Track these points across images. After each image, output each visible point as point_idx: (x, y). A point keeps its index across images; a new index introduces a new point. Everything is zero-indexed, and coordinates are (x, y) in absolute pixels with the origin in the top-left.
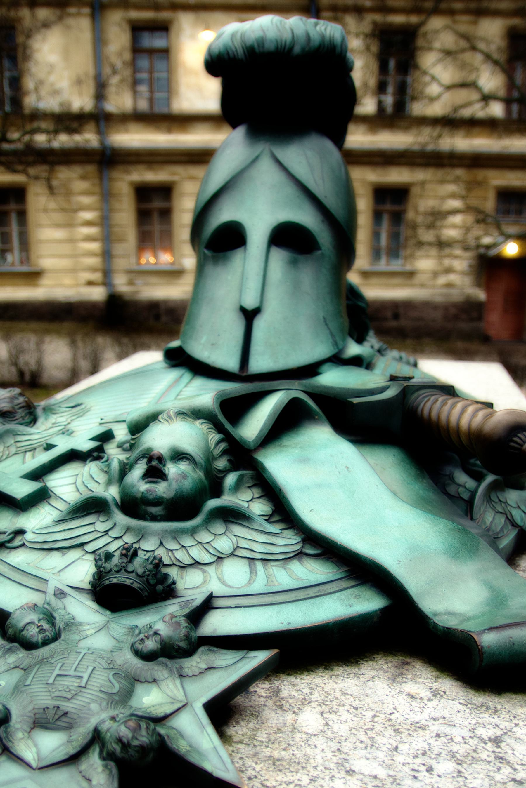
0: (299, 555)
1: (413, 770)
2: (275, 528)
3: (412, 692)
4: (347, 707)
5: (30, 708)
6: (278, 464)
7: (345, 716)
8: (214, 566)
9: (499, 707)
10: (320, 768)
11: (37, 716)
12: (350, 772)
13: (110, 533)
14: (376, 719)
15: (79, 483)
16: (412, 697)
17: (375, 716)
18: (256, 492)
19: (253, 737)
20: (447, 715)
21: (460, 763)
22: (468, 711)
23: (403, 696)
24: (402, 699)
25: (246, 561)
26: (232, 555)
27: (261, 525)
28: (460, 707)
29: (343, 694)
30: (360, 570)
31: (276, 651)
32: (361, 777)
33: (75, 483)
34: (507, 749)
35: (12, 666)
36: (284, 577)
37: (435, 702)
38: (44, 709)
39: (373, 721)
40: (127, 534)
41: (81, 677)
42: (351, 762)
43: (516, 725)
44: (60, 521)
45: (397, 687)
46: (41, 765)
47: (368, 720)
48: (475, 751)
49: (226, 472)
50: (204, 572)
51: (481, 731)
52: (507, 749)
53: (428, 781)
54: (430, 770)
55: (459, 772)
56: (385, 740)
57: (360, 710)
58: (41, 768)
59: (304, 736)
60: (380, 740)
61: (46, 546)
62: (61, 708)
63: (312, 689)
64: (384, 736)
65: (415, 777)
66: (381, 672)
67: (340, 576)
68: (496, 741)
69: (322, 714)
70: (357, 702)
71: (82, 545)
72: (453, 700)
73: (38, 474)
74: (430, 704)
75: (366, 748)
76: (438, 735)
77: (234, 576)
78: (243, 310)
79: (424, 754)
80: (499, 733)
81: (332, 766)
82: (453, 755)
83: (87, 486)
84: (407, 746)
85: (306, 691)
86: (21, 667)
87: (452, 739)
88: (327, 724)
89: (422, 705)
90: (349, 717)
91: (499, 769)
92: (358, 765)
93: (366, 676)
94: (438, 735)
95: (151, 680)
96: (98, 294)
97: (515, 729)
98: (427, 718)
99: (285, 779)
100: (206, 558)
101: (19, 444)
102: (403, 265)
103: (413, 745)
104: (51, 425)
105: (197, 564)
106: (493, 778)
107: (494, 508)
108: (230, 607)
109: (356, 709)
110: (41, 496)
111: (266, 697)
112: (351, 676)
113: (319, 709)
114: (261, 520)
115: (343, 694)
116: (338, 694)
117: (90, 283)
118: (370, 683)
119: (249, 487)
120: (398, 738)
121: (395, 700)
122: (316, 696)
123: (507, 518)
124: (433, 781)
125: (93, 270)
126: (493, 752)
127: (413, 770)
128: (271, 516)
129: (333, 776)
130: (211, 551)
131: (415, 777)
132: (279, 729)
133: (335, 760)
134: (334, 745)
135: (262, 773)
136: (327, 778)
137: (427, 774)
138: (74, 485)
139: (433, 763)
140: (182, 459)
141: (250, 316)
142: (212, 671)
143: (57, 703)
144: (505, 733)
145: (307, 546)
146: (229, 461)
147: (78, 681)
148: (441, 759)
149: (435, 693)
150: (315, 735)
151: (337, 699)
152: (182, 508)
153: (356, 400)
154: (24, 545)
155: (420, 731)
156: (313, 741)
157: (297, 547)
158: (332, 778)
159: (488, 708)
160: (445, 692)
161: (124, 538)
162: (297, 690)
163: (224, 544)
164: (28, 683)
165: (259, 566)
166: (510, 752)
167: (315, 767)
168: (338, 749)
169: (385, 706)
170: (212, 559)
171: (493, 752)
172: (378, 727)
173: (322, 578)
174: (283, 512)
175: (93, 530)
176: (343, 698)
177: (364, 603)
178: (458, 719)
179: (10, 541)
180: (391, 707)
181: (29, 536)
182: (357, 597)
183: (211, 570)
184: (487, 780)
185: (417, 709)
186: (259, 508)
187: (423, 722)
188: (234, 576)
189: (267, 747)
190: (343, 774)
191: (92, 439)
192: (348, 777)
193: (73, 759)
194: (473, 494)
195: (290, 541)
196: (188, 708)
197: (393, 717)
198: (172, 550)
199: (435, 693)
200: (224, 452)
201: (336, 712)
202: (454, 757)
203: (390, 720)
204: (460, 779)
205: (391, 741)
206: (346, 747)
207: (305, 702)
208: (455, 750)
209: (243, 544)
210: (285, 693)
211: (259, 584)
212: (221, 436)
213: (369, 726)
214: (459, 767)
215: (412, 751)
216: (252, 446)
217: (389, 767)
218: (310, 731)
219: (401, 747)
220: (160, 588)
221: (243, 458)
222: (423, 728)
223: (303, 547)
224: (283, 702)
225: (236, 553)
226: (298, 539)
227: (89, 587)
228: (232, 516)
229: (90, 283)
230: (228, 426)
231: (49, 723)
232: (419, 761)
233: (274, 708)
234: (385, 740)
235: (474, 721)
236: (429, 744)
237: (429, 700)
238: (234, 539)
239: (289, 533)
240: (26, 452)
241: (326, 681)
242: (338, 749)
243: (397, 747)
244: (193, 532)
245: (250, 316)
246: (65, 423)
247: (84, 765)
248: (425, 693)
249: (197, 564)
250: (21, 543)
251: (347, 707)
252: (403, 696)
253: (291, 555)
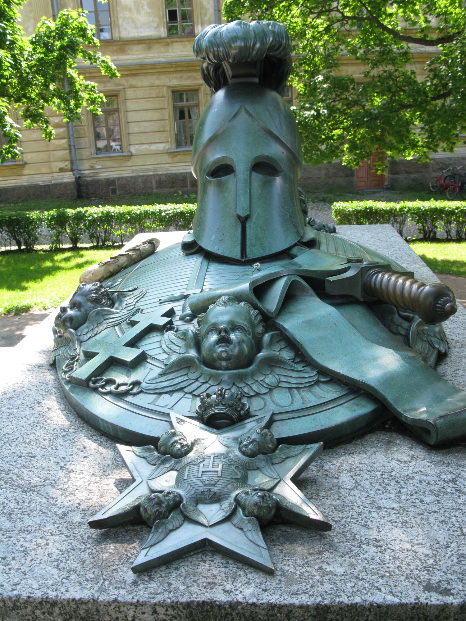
0: (317, 382)
1: (412, 502)
2: (299, 367)
3: (399, 458)
4: (365, 471)
5: (193, 492)
6: (291, 324)
7: (366, 476)
8: (268, 394)
9: (450, 462)
10: (361, 507)
11: (198, 497)
12: (379, 508)
13: (199, 380)
14: (383, 476)
15: (164, 346)
16: (400, 461)
17: (382, 475)
18: (283, 344)
19: (318, 495)
20: (422, 469)
21: (436, 495)
22: (433, 466)
23: (394, 461)
24: (394, 463)
25: (287, 390)
26: (277, 386)
27: (292, 366)
28: (428, 464)
29: (360, 464)
30: (355, 389)
31: (322, 443)
32: (386, 509)
33: (161, 347)
34: (461, 485)
35: (169, 469)
36: (311, 398)
37: (414, 463)
38: (202, 492)
39: (382, 478)
40: (211, 380)
41: (217, 472)
42: (377, 501)
43: (462, 471)
44: (161, 375)
45: (390, 457)
46: (211, 524)
47: (379, 477)
48: (443, 488)
49: (263, 334)
50: (263, 399)
51: (443, 477)
52: (461, 485)
53: (422, 508)
54: (422, 501)
55: (438, 501)
56: (392, 488)
57: (373, 472)
58: (212, 526)
59: (346, 491)
60: (390, 488)
61: (157, 391)
62: (212, 490)
63: (341, 463)
64: (390, 485)
65: (415, 506)
66: (378, 449)
67: (344, 393)
68: (454, 481)
69: (352, 477)
70: (370, 468)
71: (181, 389)
72: (423, 460)
73: (133, 343)
74: (411, 464)
75: (383, 493)
76: (421, 482)
77: (282, 400)
78: (239, 217)
79: (416, 493)
80: (454, 476)
81: (367, 505)
82: (432, 491)
83: (171, 349)
84: (405, 490)
85: (338, 464)
86: (175, 468)
87: (429, 483)
88: (356, 482)
89: (407, 465)
90: (368, 476)
91: (459, 496)
92: (382, 503)
93: (370, 452)
94: (421, 482)
95: (256, 468)
96: (68, 178)
97: (462, 473)
98: (411, 472)
99: (344, 516)
100: (264, 391)
101: (108, 321)
102: (130, 10)
103: (409, 489)
104: (125, 306)
105: (257, 394)
106: (457, 502)
107: (421, 339)
108: (285, 419)
109: (370, 472)
110: (142, 359)
111: (316, 471)
112: (361, 452)
113: (349, 474)
114: (290, 362)
115: (360, 464)
116: (357, 464)
117: (61, 170)
118: (373, 456)
119: (277, 342)
120: (399, 485)
121: (391, 464)
122: (345, 467)
123: (430, 344)
124: (425, 507)
125: (64, 160)
126: (453, 487)
127: (412, 502)
128: (294, 359)
129: (370, 511)
130: (265, 386)
131: (415, 506)
132: (330, 489)
133: (368, 502)
134: (365, 494)
135: (331, 513)
136: (367, 512)
137: (421, 504)
138: (160, 349)
139: (422, 497)
140: (237, 329)
141: (243, 221)
142: (288, 459)
143: (209, 488)
144: (457, 476)
145: (321, 376)
146: (263, 326)
147: (216, 473)
148: (426, 495)
149: (413, 457)
150: (352, 489)
151: (357, 467)
152: (243, 362)
153: (332, 279)
154: (141, 392)
155: (410, 480)
156: (352, 492)
157: (316, 378)
158: (370, 512)
159: (444, 463)
160: (417, 456)
161: (209, 382)
162: (333, 465)
163: (270, 379)
164: (186, 478)
165: (295, 391)
166: (462, 486)
167: (358, 507)
168: (368, 496)
169: (386, 468)
170: (267, 391)
171: (453, 487)
172: (386, 481)
173: (334, 396)
174: (301, 356)
175: (187, 378)
176: (361, 466)
177: (363, 408)
178: (429, 471)
179: (131, 389)
180: (390, 468)
181: (144, 385)
182: (357, 405)
183: (267, 397)
184: (454, 503)
185: (404, 468)
186: (287, 355)
187: (410, 475)
188: (282, 400)
189: (327, 499)
190: (375, 509)
191: (163, 316)
192: (379, 511)
193: (227, 519)
194: (408, 330)
195: (310, 375)
196: (282, 482)
197: (392, 474)
198: (241, 387)
199: (413, 457)
200: (260, 321)
201: (359, 475)
202: (433, 493)
203: (391, 476)
204: (439, 504)
205: (395, 488)
206: (372, 493)
207: (340, 471)
208: (432, 488)
209: (283, 379)
210: (326, 467)
211: (298, 405)
212: (257, 311)
213: (381, 481)
214: (437, 498)
215: (409, 492)
216: (274, 315)
217: (399, 502)
218: (348, 487)
219: (402, 490)
220: (242, 412)
221: (269, 321)
222: (412, 478)
223: (318, 378)
224: (327, 473)
225: (280, 385)
226: (315, 373)
227: (195, 415)
228: (272, 363)
229: (61, 170)
230: (259, 305)
231: (207, 500)
232: (414, 497)
233: (323, 476)
234: (392, 488)
235: (438, 472)
236: (417, 487)
237: (410, 462)
238: (277, 377)
239: (308, 369)
240: (114, 326)
241: (348, 457)
242: (368, 496)
243: (400, 491)
244: (253, 374)
245: (243, 221)
246: (134, 303)
247: (236, 520)
248: (407, 459)
249: (257, 394)
250: (140, 390)
251: (365, 471)
252: (394, 461)
253: (313, 383)
